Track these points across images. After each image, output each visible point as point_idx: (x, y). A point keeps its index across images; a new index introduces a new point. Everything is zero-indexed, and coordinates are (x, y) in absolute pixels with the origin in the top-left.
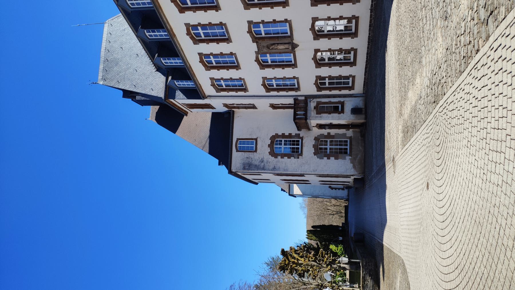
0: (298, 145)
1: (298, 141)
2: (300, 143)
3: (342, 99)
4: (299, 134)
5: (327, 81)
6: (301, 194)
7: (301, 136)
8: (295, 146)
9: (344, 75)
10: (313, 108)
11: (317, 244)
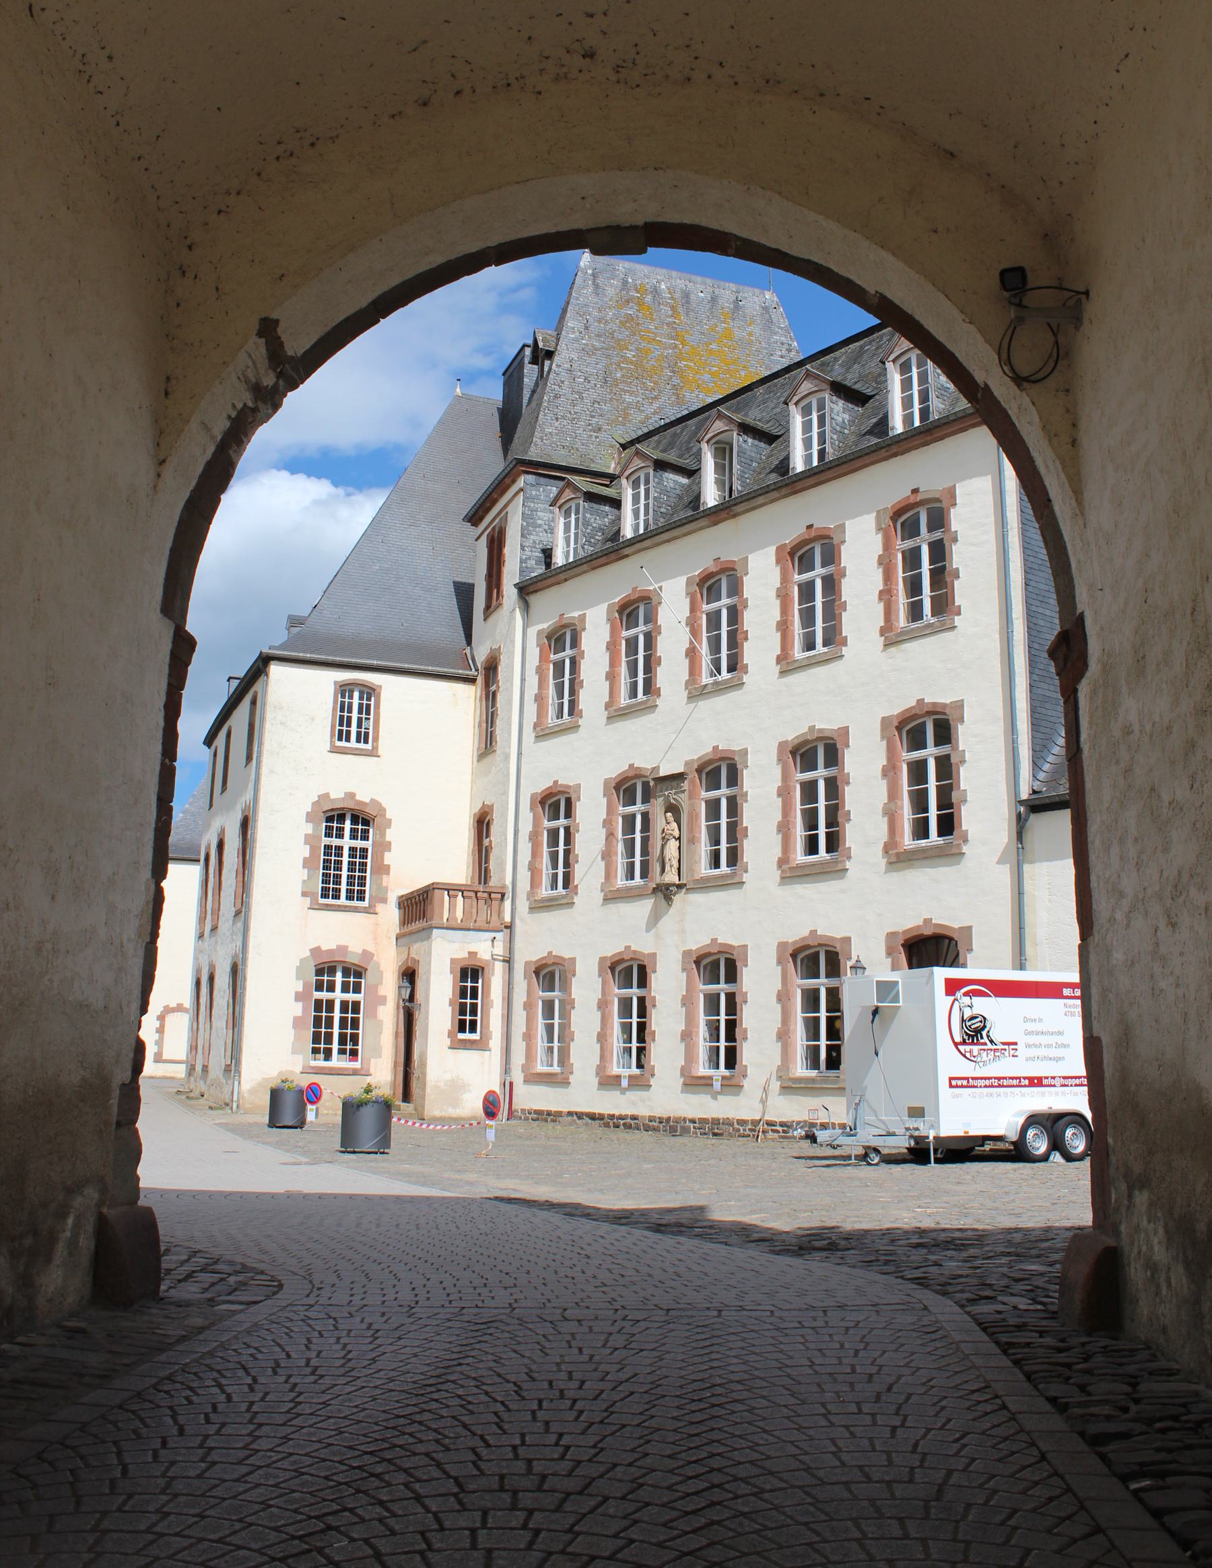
0: (349, 898)
1: (362, 899)
2: (355, 903)
3: (496, 1042)
4: (384, 900)
5: (562, 821)
6: (874, 321)
7: (380, 908)
9: (574, 1048)
10: (473, 948)
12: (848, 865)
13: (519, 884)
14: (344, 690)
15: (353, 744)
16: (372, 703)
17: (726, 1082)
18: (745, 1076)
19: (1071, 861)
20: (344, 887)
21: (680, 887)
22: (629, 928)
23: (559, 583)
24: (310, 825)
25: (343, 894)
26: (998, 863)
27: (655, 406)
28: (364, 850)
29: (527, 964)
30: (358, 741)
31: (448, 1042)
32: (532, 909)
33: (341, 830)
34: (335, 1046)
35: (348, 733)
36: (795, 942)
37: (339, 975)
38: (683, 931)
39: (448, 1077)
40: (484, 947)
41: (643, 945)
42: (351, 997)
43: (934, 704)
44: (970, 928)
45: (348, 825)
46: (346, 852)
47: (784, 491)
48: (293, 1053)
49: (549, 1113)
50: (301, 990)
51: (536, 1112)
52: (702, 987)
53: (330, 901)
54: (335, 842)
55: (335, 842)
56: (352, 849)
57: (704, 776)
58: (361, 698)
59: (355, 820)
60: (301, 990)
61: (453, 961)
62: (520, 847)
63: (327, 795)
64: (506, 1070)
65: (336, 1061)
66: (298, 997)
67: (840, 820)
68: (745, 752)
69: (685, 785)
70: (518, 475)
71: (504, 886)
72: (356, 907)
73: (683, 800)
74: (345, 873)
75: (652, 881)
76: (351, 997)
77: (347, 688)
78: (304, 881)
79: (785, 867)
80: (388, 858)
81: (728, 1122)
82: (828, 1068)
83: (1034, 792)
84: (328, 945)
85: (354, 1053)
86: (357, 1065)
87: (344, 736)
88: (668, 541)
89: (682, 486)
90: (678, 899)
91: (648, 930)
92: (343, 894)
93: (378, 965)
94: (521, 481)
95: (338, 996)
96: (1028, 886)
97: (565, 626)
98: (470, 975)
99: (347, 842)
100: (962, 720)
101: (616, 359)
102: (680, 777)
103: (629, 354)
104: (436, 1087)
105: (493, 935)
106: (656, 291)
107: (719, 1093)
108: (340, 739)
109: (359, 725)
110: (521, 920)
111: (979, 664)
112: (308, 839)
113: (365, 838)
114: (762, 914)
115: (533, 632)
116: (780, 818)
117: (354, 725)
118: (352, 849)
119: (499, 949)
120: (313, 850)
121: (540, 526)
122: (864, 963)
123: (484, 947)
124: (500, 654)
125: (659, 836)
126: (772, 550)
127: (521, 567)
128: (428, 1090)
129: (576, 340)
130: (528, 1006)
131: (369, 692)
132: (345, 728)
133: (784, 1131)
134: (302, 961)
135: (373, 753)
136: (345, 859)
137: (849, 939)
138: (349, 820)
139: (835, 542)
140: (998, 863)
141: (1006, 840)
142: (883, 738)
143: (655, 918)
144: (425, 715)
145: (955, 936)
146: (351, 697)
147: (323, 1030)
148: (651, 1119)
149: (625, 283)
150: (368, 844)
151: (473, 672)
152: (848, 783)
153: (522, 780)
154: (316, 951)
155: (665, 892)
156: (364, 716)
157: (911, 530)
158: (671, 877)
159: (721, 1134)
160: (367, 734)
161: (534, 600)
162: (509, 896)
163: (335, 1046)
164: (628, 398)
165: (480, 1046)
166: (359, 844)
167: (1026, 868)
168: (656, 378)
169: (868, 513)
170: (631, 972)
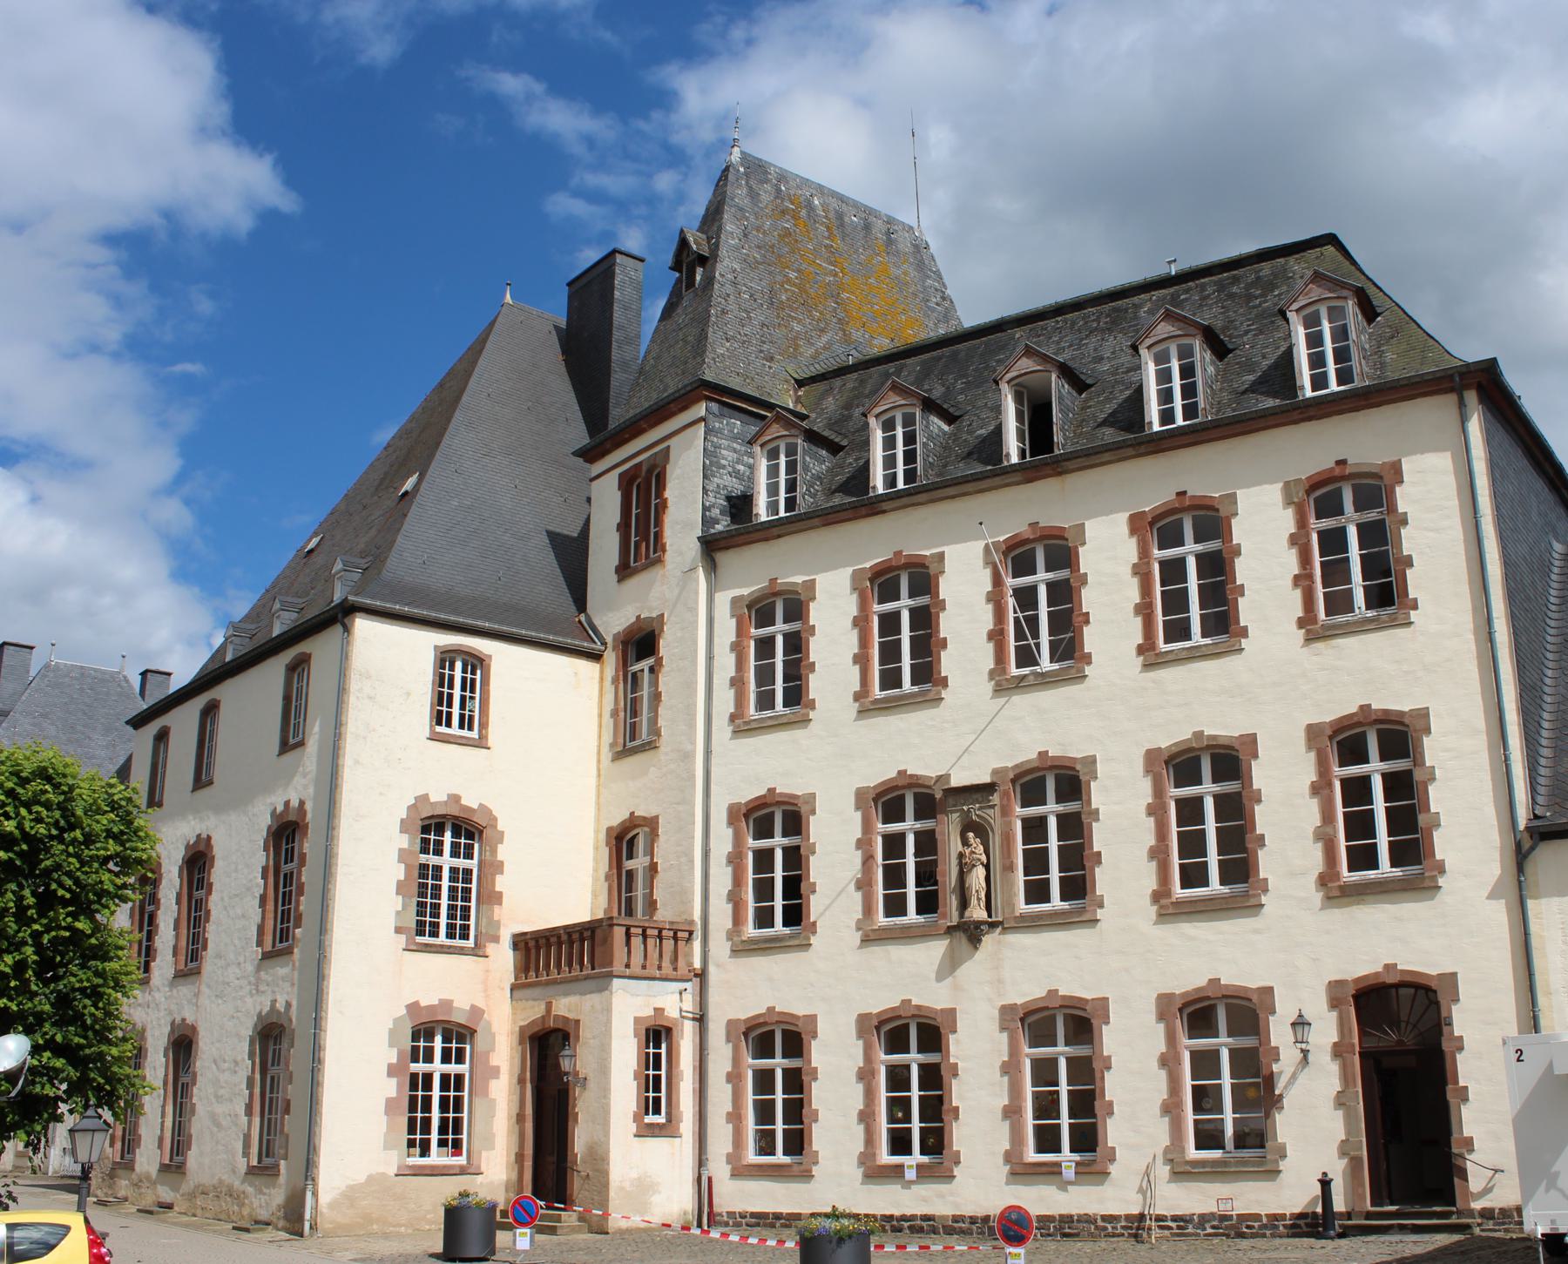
1: (465, 937)
2: (458, 942)
3: (687, 1125)
4: (496, 939)
7: (491, 948)
8: (1379, 806)
11: (288, 1005)
12: (1264, 899)
13: (712, 920)
14: (445, 658)
15: (455, 730)
16: (478, 677)
17: (1081, 1169)
18: (1112, 1160)
19: (588, 919)
20: (443, 921)
21: (993, 925)
22: (911, 974)
23: (766, 539)
24: (405, 837)
25: (443, 930)
26: (1488, 898)
27: (825, 339)
28: (468, 872)
29: (731, 1024)
30: (461, 726)
31: (633, 1128)
32: (736, 952)
33: (439, 844)
34: (434, 1136)
35: (449, 715)
36: (1187, 993)
37: (438, 1039)
38: (1000, 981)
39: (634, 1174)
40: (672, 1000)
41: (933, 997)
42: (453, 1068)
43: (1386, 711)
44: (1454, 975)
45: (448, 838)
46: (446, 874)
47: (1142, 449)
48: (385, 1148)
49: (778, 1216)
50: (394, 1061)
51: (753, 1215)
52: (1027, 1050)
53: (427, 939)
54: (432, 860)
55: (432, 860)
56: (454, 870)
57: (1018, 789)
58: (464, 671)
59: (456, 833)
60: (394, 1061)
61: (637, 1020)
62: (712, 871)
63: (425, 797)
64: (701, 1162)
65: (437, 1157)
66: (392, 1071)
67: (1249, 846)
68: (1092, 761)
69: (995, 799)
70: (697, 401)
71: (692, 922)
72: (462, 948)
73: (993, 816)
74: (444, 902)
75: (944, 916)
76: (453, 1068)
77: (447, 656)
78: (398, 913)
79: (1164, 902)
80: (501, 883)
81: (1088, 1219)
82: (1237, 1147)
83: (1536, 817)
84: (428, 999)
85: (457, 1145)
86: (462, 1160)
87: (440, 718)
88: (953, 497)
89: (945, 433)
90: (989, 940)
91: (940, 977)
92: (443, 930)
93: (489, 1024)
94: (701, 409)
95: (438, 1067)
96: (1534, 927)
97: (775, 594)
98: (656, 1035)
99: (446, 861)
100: (1428, 731)
101: (779, 278)
102: (989, 788)
103: (793, 275)
104: (622, 1188)
105: (682, 985)
106: (810, 207)
107: (1071, 1183)
108: (439, 723)
109: (463, 706)
110: (718, 966)
111: (1440, 664)
112: (403, 856)
113: (469, 856)
114: (1130, 956)
115: (724, 599)
116: (1153, 842)
117: (457, 704)
118: (454, 870)
119: (689, 1004)
120: (408, 868)
121: (724, 467)
122: (1308, 1017)
123: (672, 1000)
124: (662, 624)
125: (954, 862)
126: (1122, 519)
127: (704, 515)
128: (612, 1194)
129: (737, 249)
130: (734, 1078)
131: (476, 662)
132: (445, 709)
133: (1179, 1227)
134: (396, 1021)
135: (481, 743)
136: (445, 884)
137: (1271, 989)
138: (450, 830)
139: (1223, 513)
140: (1488, 898)
141: (1497, 872)
142: (1309, 748)
143: (951, 965)
144: (547, 699)
145: (1433, 985)
146: (452, 668)
147: (419, 1115)
148: (956, 1219)
149: (779, 191)
150: (473, 864)
151: (599, 646)
152: (1259, 801)
153: (713, 787)
154: (413, 1008)
155: (972, 933)
156: (468, 694)
157: (1329, 506)
158: (978, 913)
159: (1077, 1235)
160: (471, 718)
161: (723, 558)
162: (698, 934)
163: (434, 1136)
164: (797, 327)
165: (668, 1130)
166: (461, 863)
167: (1530, 903)
168: (821, 307)
169: (1272, 482)
170: (912, 1035)
